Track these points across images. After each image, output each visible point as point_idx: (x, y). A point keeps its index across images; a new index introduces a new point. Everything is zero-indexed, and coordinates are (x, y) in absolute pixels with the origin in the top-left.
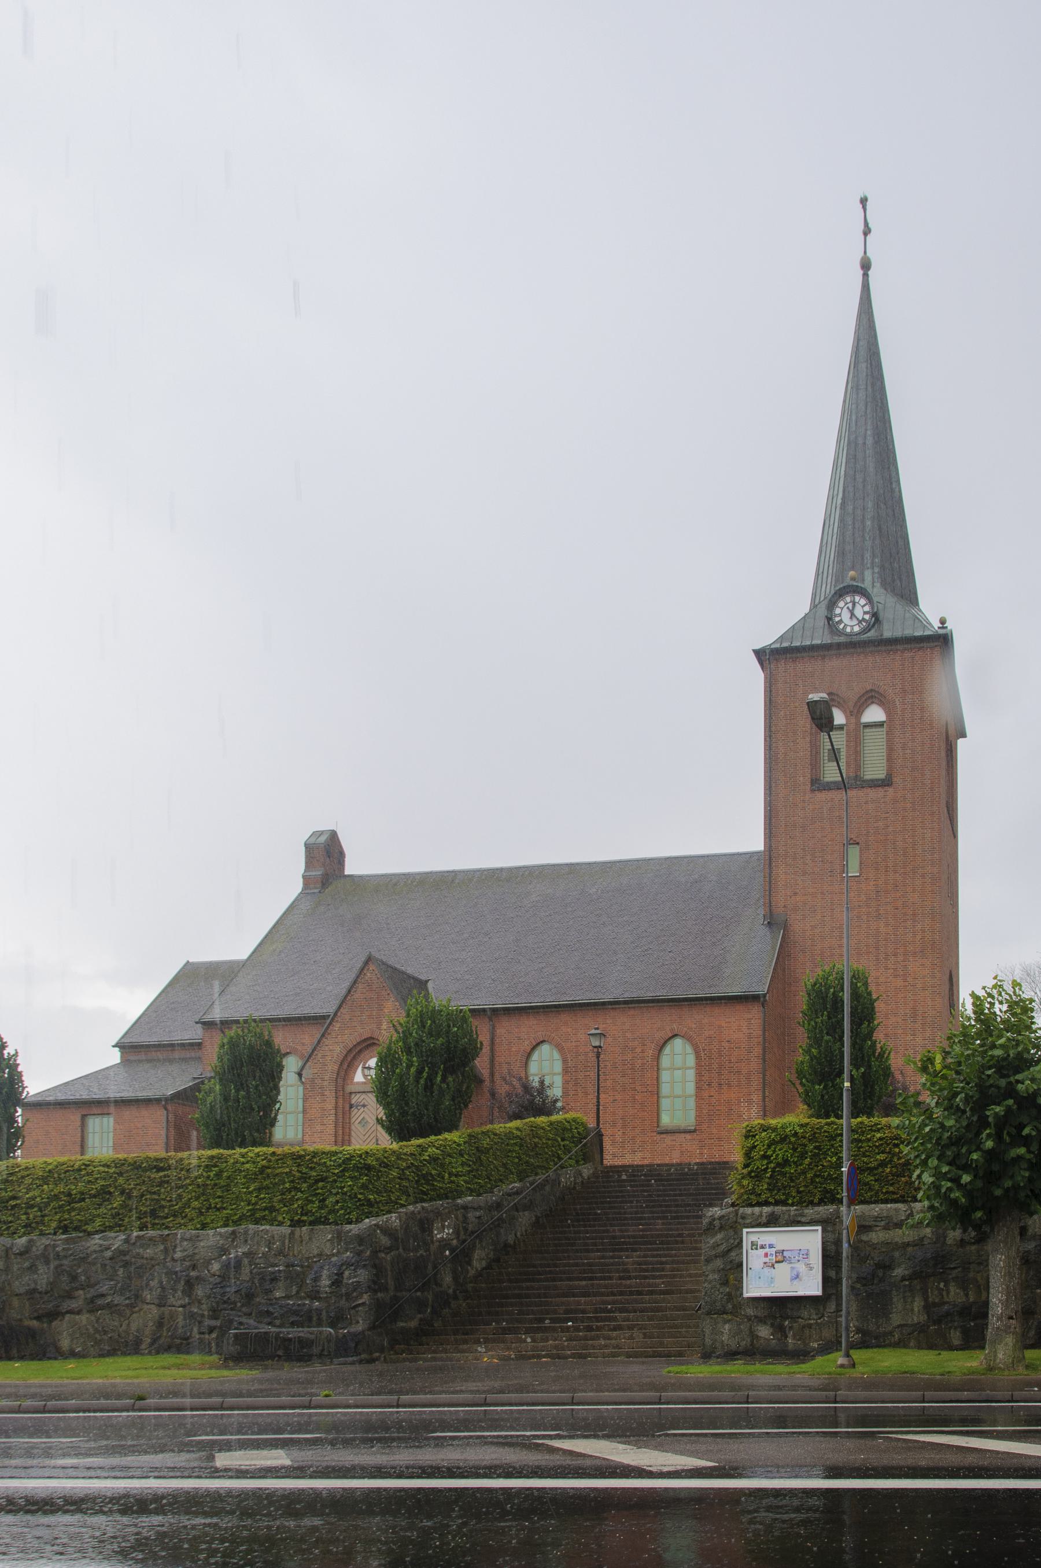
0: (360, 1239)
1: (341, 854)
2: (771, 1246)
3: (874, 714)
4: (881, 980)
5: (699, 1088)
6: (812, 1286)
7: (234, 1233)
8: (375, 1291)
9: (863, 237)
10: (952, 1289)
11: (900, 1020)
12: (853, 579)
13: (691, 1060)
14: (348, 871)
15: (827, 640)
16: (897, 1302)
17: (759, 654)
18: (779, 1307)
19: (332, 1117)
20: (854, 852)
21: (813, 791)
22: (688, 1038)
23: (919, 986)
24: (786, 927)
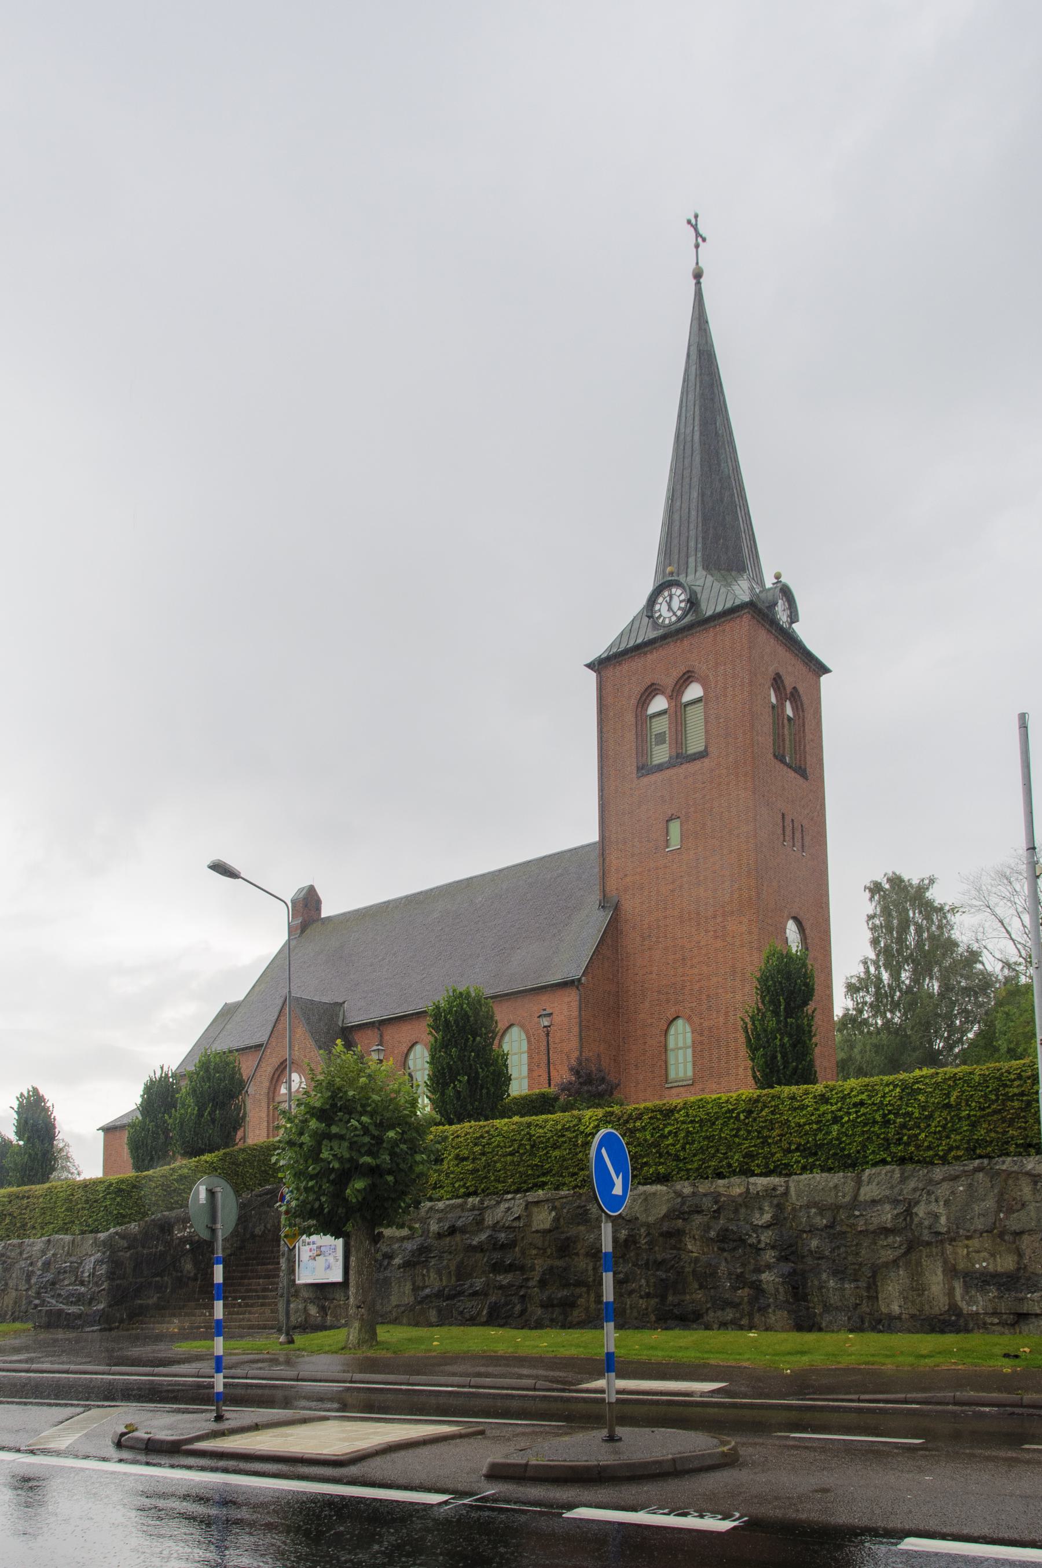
0: (104, 1243)
1: (318, 902)
2: (314, 1243)
3: (694, 691)
4: (702, 943)
5: (530, 1070)
6: (336, 1276)
7: (49, 1241)
8: (113, 1279)
9: (694, 250)
10: (432, 1275)
11: (720, 980)
12: (671, 574)
13: (525, 1046)
14: (325, 913)
15: (652, 635)
16: (395, 1289)
17: (590, 666)
18: (322, 1289)
19: (265, 1124)
20: (675, 828)
21: (638, 778)
22: (522, 1026)
23: (738, 943)
24: (617, 908)
